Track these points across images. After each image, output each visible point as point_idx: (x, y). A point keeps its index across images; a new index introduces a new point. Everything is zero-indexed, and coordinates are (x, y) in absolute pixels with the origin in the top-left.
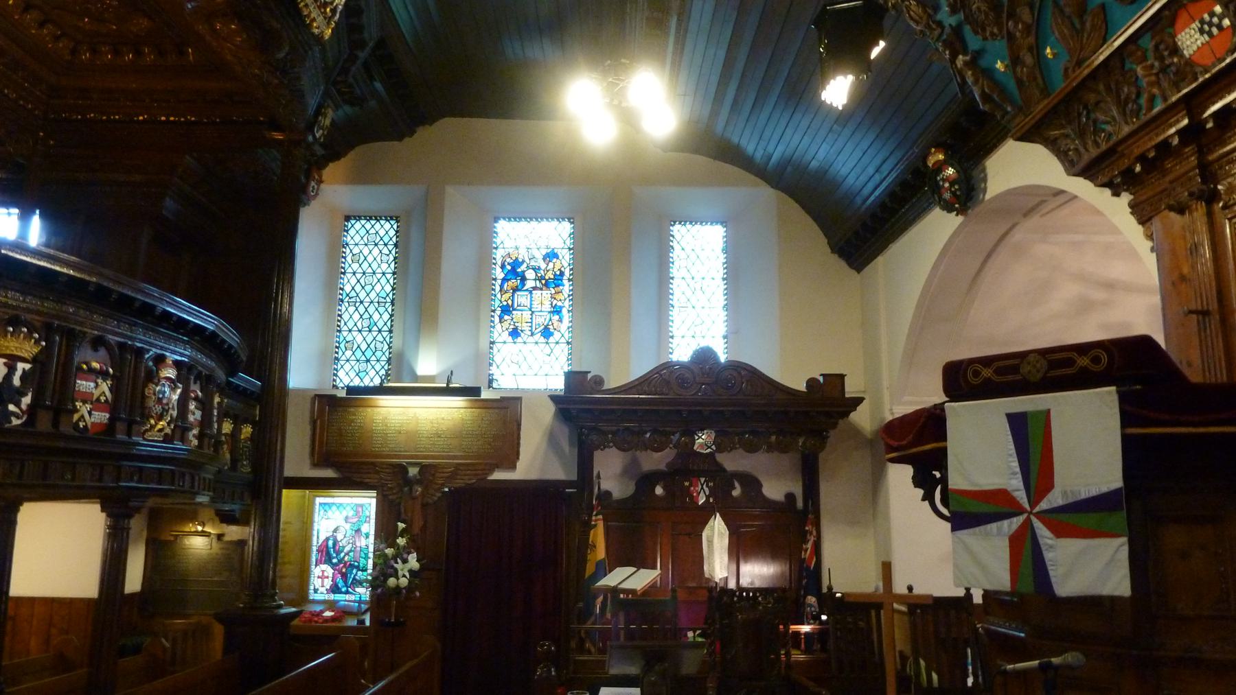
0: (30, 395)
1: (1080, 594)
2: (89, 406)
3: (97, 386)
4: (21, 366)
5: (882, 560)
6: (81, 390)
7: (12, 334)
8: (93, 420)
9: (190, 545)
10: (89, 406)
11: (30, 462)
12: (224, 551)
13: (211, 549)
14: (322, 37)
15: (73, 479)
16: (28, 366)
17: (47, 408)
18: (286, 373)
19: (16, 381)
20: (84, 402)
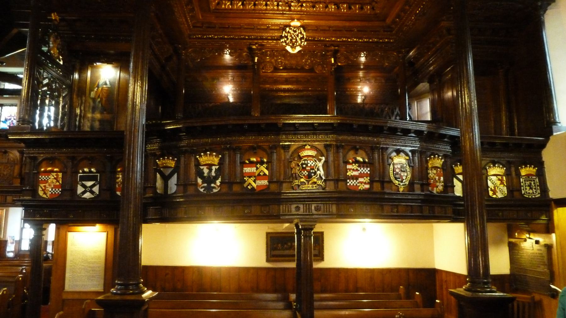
0: (220, 179)
1: (283, 263)
2: (253, 179)
3: (257, 169)
4: (214, 168)
5: (266, 231)
6: (246, 172)
7: (171, 160)
8: (257, 184)
9: (524, 247)
10: (253, 179)
11: (428, 207)
12: (540, 252)
13: (533, 250)
14: (31, 265)
15: (397, 212)
16: (217, 167)
17: (377, 181)
18: (552, 103)
19: (213, 174)
20: (250, 177)
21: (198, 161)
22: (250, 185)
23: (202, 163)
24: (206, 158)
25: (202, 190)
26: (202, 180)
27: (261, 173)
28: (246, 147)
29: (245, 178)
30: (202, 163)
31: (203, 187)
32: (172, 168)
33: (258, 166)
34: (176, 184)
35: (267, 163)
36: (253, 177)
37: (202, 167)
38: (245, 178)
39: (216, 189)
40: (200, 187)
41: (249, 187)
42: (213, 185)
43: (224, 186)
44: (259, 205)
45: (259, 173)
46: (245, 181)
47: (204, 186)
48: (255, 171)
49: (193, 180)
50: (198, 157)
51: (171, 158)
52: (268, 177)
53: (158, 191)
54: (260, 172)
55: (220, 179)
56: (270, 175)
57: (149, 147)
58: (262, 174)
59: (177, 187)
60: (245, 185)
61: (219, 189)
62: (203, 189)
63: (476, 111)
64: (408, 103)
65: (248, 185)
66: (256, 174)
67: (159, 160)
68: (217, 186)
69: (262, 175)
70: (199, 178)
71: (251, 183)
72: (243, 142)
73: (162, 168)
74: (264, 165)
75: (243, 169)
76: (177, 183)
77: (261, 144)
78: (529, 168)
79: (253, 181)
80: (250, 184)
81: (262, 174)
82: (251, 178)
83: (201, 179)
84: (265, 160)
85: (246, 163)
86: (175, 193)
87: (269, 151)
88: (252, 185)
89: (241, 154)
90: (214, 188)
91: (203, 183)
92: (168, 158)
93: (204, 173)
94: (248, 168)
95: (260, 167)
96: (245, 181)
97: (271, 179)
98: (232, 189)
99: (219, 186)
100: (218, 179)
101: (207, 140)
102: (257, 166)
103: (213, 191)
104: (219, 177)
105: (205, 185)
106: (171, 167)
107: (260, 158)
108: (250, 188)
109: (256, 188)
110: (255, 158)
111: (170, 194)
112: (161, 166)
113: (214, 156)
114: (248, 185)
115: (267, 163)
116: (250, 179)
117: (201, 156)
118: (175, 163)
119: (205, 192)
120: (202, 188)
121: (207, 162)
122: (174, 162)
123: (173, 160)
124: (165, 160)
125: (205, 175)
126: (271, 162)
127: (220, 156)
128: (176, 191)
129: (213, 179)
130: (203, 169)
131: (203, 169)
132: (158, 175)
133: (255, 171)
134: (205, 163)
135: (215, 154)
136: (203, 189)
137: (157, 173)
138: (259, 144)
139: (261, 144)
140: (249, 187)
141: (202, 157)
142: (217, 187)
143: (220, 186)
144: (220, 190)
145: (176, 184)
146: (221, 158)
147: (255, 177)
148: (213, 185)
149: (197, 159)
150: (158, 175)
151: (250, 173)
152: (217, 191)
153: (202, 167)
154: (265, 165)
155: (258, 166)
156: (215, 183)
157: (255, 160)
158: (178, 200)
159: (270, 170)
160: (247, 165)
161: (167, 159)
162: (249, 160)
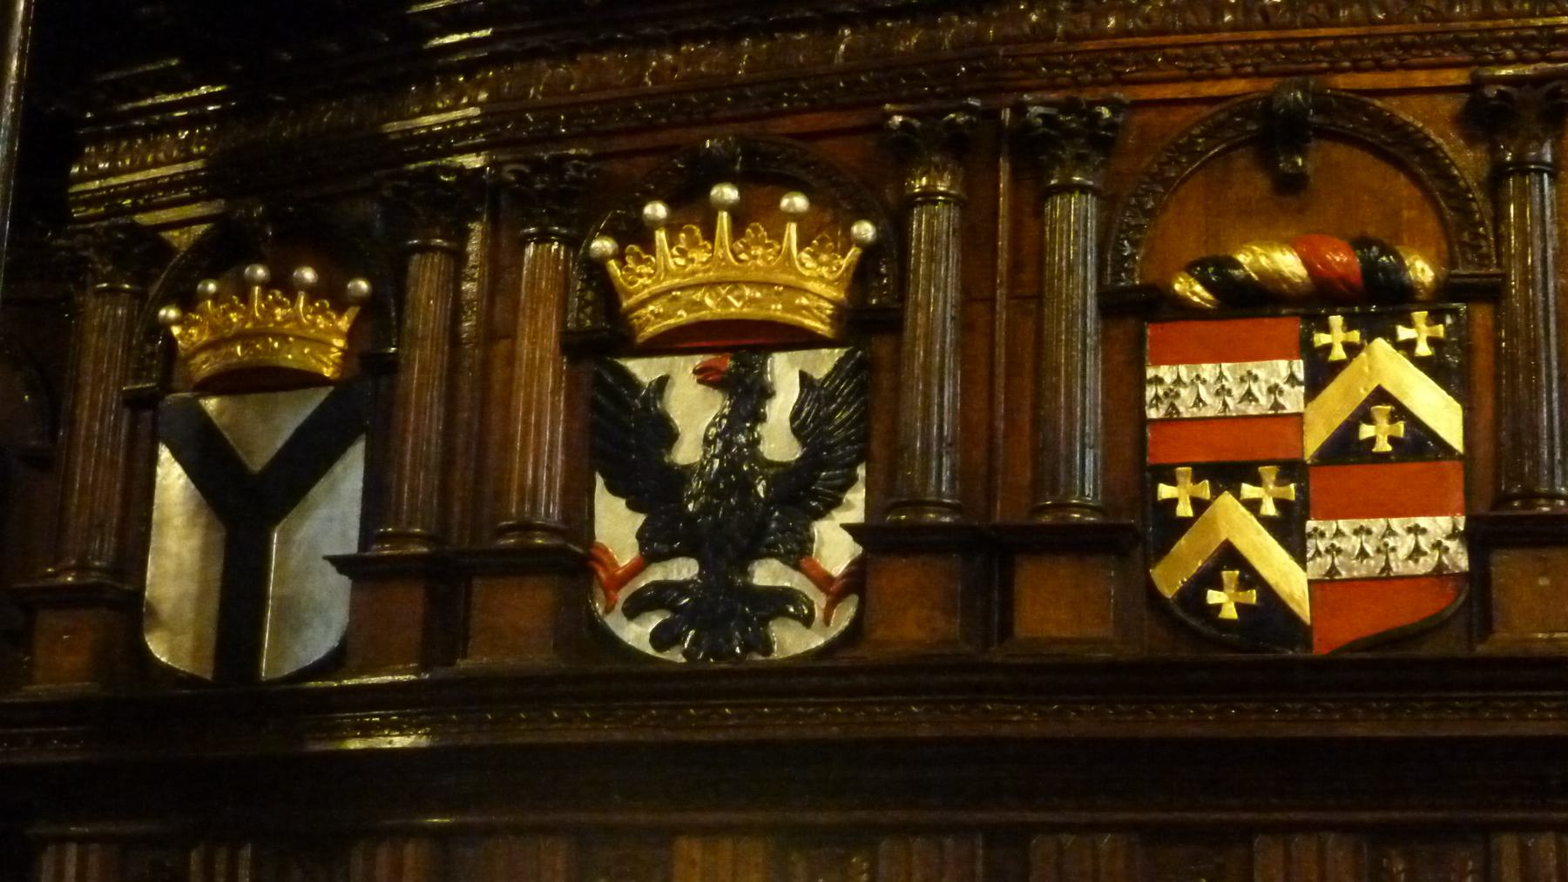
0: (857, 498)
2: (1267, 494)
3: (1321, 373)
7: (314, 293)
8: (1318, 567)
16: (823, 362)
21: (606, 293)
22: (1231, 576)
23: (653, 320)
24: (701, 256)
25: (637, 633)
26: (640, 519)
27: (1366, 431)
28: (1179, 116)
29: (1165, 491)
30: (653, 320)
31: (657, 597)
32: (319, 381)
33: (1335, 336)
34: (342, 564)
35: (1440, 301)
36: (1269, 473)
37: (643, 370)
38: (1165, 491)
39: (807, 621)
40: (623, 595)
41: (1214, 597)
42: (767, 574)
43: (902, 575)
44: (1347, 829)
45: (1348, 429)
46: (1171, 527)
47: (662, 587)
48: (1293, 400)
49: (551, 510)
50: (603, 245)
51: (309, 275)
52: (1454, 475)
53: (158, 647)
54: (1364, 414)
55: (857, 498)
56: (1484, 449)
57: (104, 175)
58: (1379, 433)
59: (354, 589)
60: (1170, 578)
61: (844, 616)
62: (654, 620)
63: (240, 452)
64: (276, 564)
65: (1209, 578)
66: (1314, 441)
67: (188, 302)
68: (823, 581)
69: (1383, 446)
70: (614, 489)
71: (1241, 544)
72: (1143, 55)
73: (210, 386)
74: (1404, 333)
75: (1141, 382)
76: (366, 538)
77: (1366, 80)
78: (738, 229)
79: (1268, 523)
80: (1229, 556)
81: (1379, 433)
82: (1248, 491)
83: (633, 506)
84: (1422, 271)
85: (1184, 310)
86: (334, 662)
87: (1467, 161)
88: (1251, 578)
89: (1109, 202)
90: (779, 602)
91: (653, 547)
92: (282, 282)
93: (667, 434)
94: (1208, 370)
95: (1352, 350)
96: (1171, 527)
97: (1503, 500)
98: (1008, 606)
99: (837, 590)
100: (833, 502)
101: (720, 55)
102: (1321, 339)
103: (767, 647)
104: (850, 482)
105: (684, 569)
106: (310, 380)
107: (1360, 243)
108: (1230, 612)
109: (1303, 609)
110: (1293, 244)
111: (271, 683)
112: (204, 366)
113: (792, 230)
114: (1209, 578)
115: (1440, 301)
116: (1227, 498)
117: (637, 235)
118: (350, 336)
119: (676, 656)
120: (635, 608)
121: (711, 306)
122: (344, 324)
123: (330, 294)
124: (246, 298)
125: (687, 452)
126: (1491, 292)
127: (865, 230)
128: (344, 642)
129: (771, 501)
130: (662, 383)
131: (662, 383)
132: (171, 477)
133: (1293, 400)
134: (683, 317)
135: (799, 202)
136: (654, 620)
137: (165, 454)
138: (1341, 81)
139: (1366, 80)
140: (1214, 597)
141: (648, 245)
142: (820, 601)
143: (857, 579)
144: (853, 634)
145: (342, 564)
146: (871, 252)
147: (1291, 469)
148: (767, 574)
149: (595, 269)
150: (171, 477)
151: (1223, 420)
152: (816, 641)
153: (643, 370)
154: (1420, 331)
155: (1335, 336)
156: (799, 553)
157: (1288, 263)
158: (355, 744)
159: (1486, 400)
160: (1199, 327)
161: (267, 286)
162: (1217, 270)
